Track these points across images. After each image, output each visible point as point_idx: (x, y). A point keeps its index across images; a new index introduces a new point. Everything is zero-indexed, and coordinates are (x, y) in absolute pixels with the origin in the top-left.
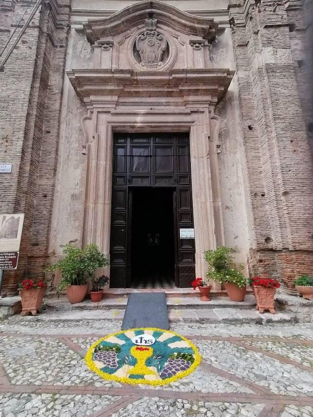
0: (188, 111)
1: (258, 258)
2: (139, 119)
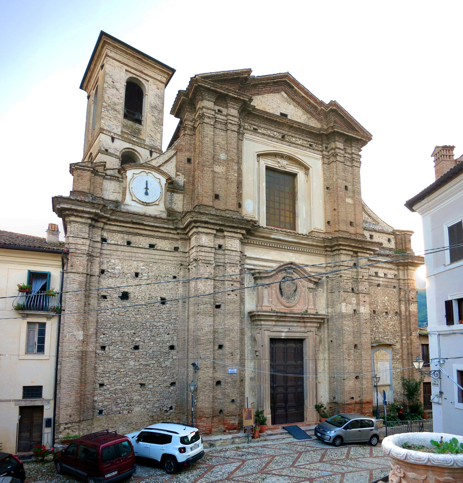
0: (306, 331)
1: (330, 406)
2: (283, 334)
